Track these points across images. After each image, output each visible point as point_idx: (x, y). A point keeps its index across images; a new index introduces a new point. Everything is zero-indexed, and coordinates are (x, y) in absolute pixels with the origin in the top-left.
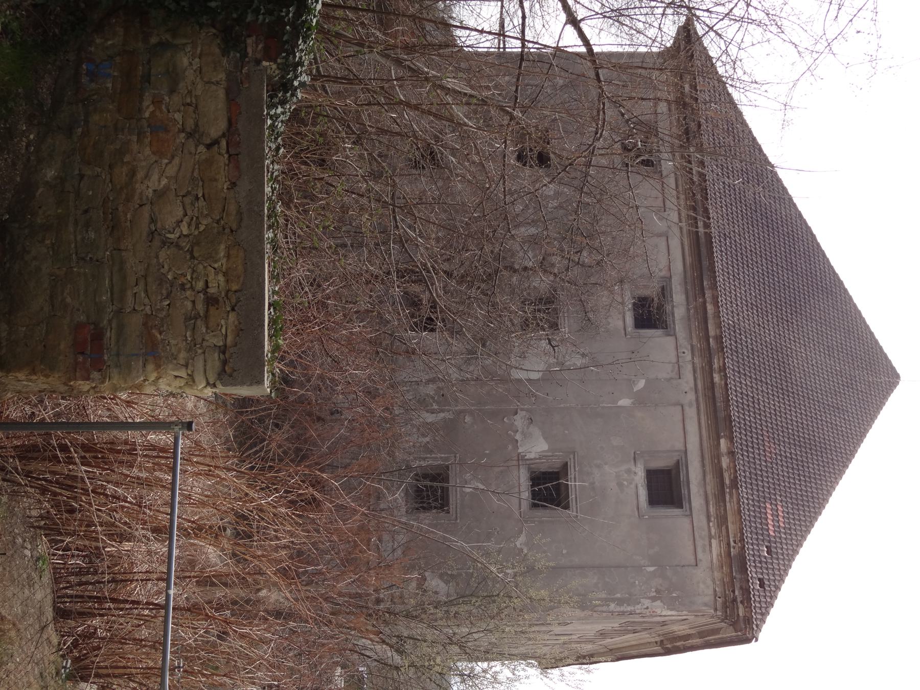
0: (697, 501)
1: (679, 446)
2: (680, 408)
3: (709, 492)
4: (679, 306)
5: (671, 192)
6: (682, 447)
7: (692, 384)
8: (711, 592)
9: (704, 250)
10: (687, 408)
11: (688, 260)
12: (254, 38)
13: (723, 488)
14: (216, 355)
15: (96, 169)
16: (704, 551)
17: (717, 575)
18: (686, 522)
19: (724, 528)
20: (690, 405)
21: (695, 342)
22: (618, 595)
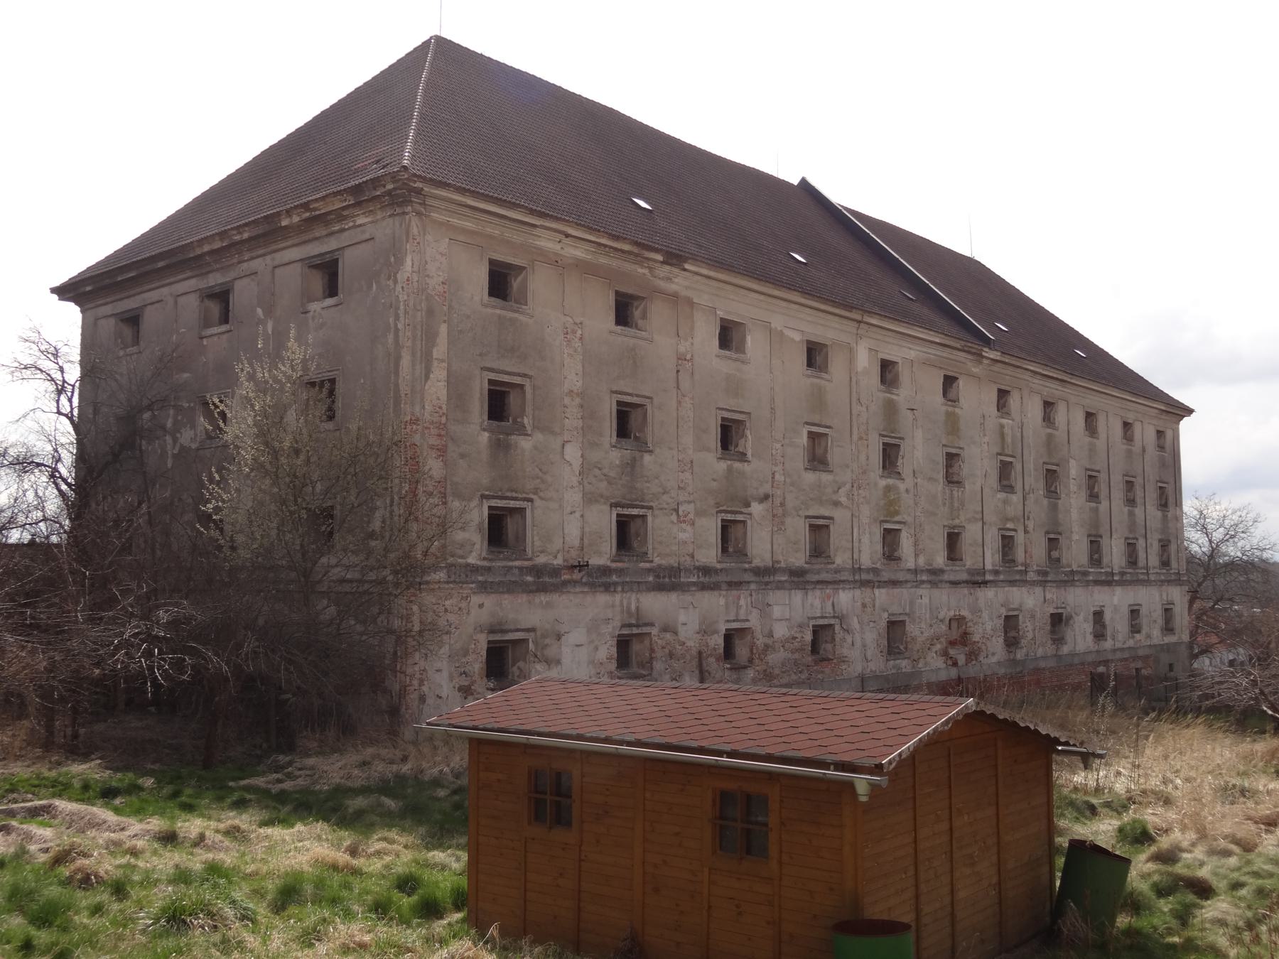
0: (332, 244)
1: (298, 266)
2: (277, 270)
3: (324, 233)
4: (215, 280)
5: (345, 239)
6: (299, 264)
7: (260, 260)
8: (390, 220)
9: (174, 260)
10: (277, 263)
11: (189, 274)
12: (322, 617)
13: (316, 221)
14: (525, 444)
15: (442, 651)
16: (363, 232)
17: (379, 215)
18: (348, 253)
19: (345, 213)
20: (273, 259)
21: (235, 261)
22: (391, 320)
